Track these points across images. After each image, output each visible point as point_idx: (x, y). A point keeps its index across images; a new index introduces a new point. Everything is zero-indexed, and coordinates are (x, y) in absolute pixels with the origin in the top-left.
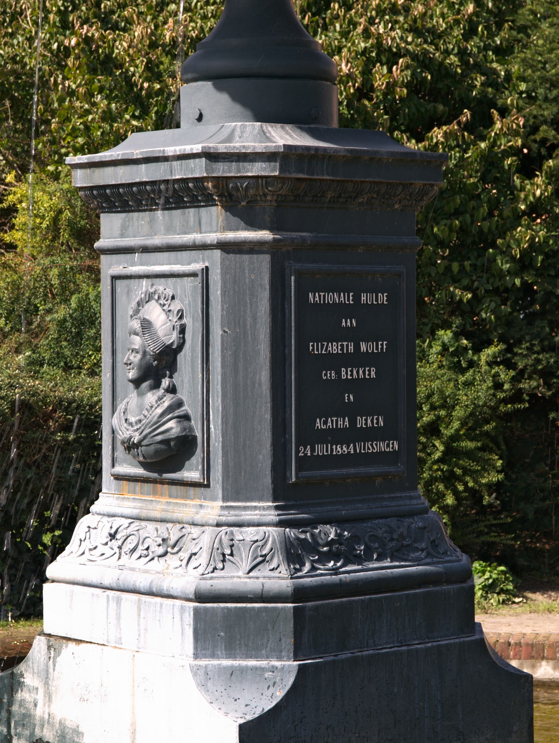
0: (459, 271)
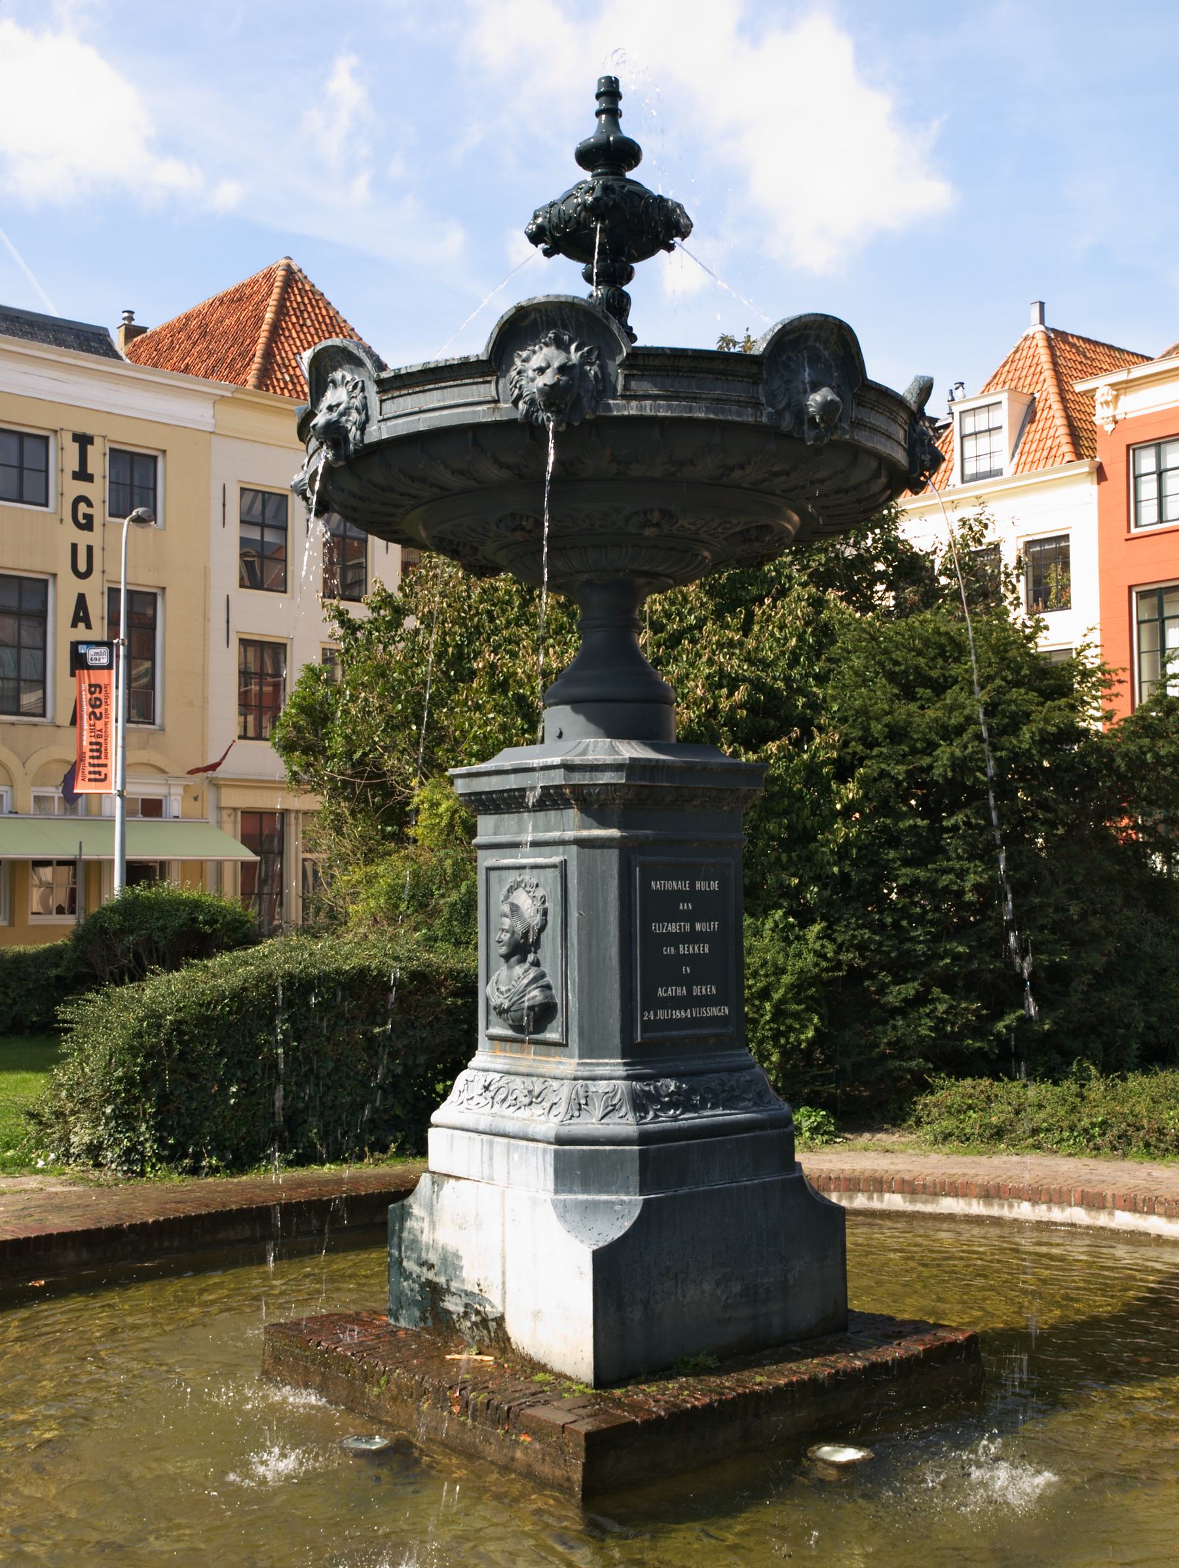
0: (788, 861)
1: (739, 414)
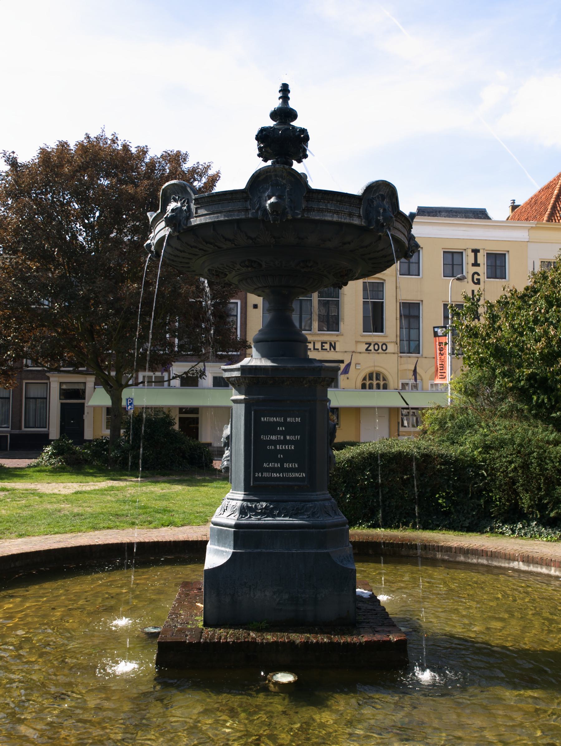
1: (238, 216)
